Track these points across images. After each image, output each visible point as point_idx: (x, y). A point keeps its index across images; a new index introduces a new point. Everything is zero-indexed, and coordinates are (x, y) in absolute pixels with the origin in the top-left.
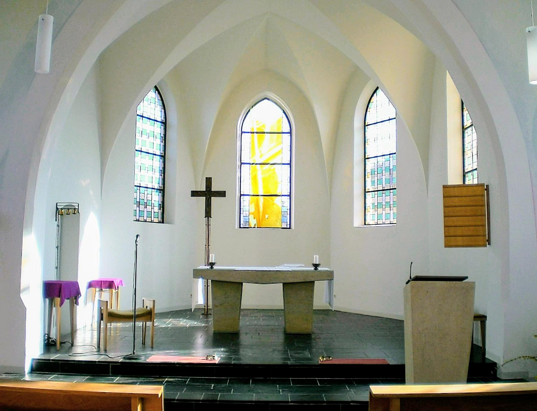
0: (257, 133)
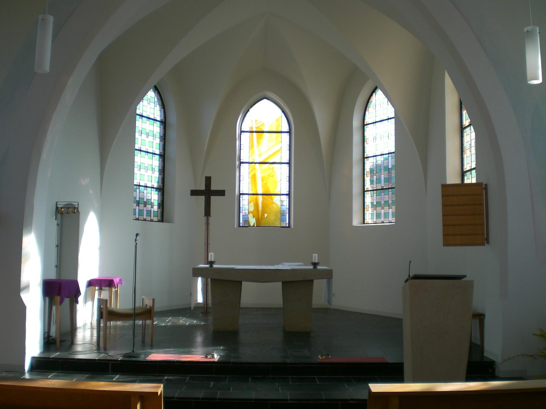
0: (256, 132)
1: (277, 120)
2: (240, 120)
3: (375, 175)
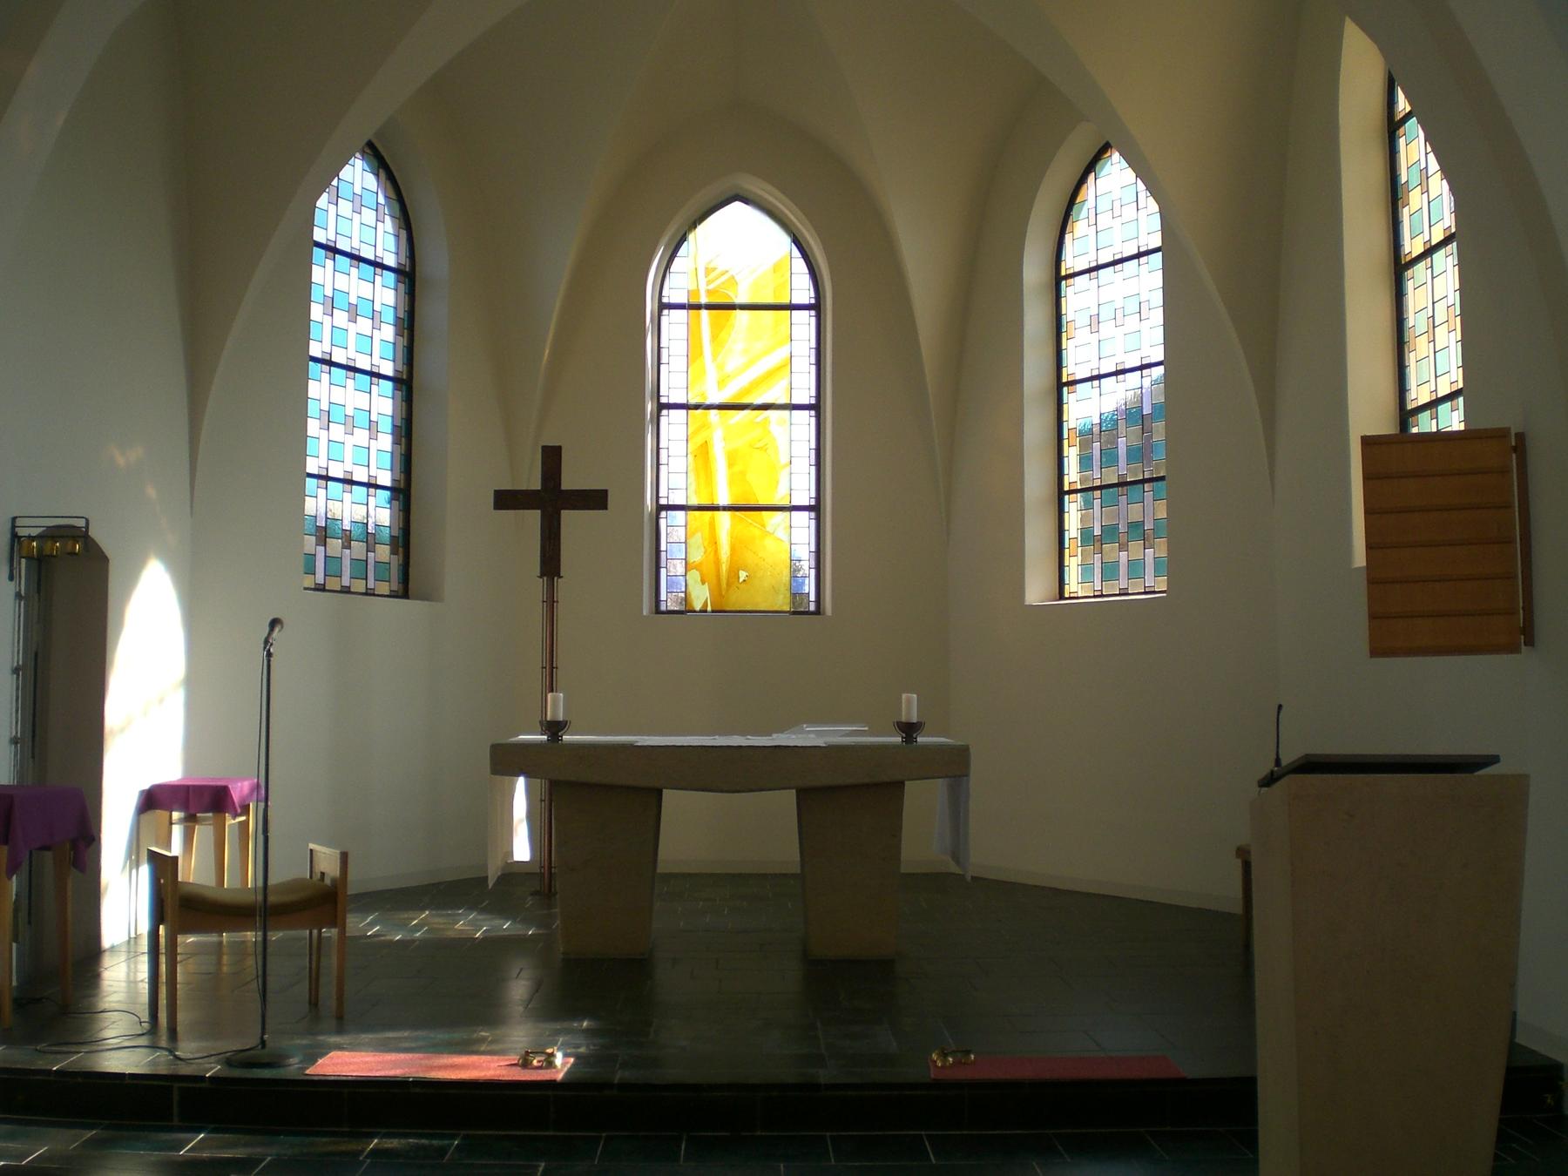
0: (709, 307)
1: (776, 268)
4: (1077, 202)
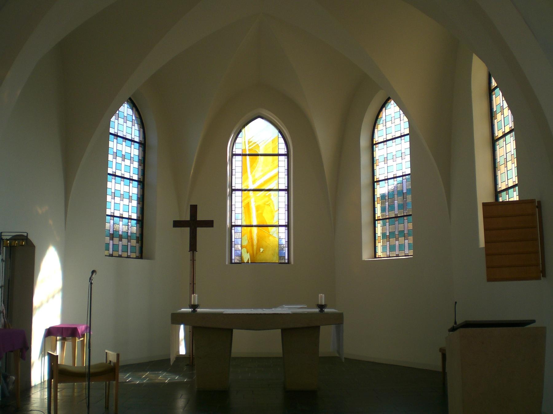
0: (249, 155)
1: (273, 141)
2: (232, 140)
3: (387, 201)
4: (379, 118)
